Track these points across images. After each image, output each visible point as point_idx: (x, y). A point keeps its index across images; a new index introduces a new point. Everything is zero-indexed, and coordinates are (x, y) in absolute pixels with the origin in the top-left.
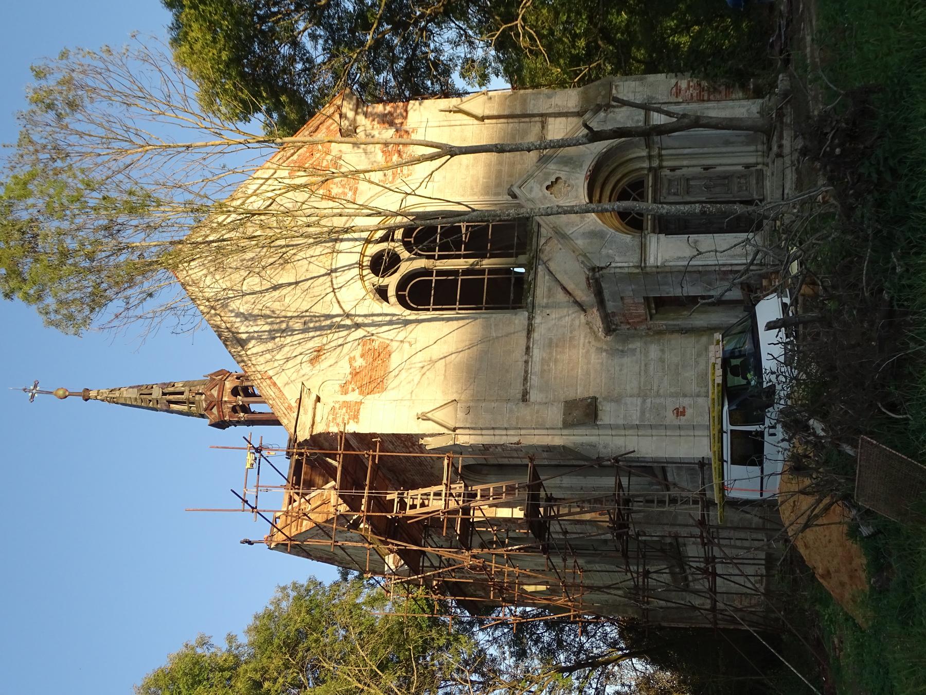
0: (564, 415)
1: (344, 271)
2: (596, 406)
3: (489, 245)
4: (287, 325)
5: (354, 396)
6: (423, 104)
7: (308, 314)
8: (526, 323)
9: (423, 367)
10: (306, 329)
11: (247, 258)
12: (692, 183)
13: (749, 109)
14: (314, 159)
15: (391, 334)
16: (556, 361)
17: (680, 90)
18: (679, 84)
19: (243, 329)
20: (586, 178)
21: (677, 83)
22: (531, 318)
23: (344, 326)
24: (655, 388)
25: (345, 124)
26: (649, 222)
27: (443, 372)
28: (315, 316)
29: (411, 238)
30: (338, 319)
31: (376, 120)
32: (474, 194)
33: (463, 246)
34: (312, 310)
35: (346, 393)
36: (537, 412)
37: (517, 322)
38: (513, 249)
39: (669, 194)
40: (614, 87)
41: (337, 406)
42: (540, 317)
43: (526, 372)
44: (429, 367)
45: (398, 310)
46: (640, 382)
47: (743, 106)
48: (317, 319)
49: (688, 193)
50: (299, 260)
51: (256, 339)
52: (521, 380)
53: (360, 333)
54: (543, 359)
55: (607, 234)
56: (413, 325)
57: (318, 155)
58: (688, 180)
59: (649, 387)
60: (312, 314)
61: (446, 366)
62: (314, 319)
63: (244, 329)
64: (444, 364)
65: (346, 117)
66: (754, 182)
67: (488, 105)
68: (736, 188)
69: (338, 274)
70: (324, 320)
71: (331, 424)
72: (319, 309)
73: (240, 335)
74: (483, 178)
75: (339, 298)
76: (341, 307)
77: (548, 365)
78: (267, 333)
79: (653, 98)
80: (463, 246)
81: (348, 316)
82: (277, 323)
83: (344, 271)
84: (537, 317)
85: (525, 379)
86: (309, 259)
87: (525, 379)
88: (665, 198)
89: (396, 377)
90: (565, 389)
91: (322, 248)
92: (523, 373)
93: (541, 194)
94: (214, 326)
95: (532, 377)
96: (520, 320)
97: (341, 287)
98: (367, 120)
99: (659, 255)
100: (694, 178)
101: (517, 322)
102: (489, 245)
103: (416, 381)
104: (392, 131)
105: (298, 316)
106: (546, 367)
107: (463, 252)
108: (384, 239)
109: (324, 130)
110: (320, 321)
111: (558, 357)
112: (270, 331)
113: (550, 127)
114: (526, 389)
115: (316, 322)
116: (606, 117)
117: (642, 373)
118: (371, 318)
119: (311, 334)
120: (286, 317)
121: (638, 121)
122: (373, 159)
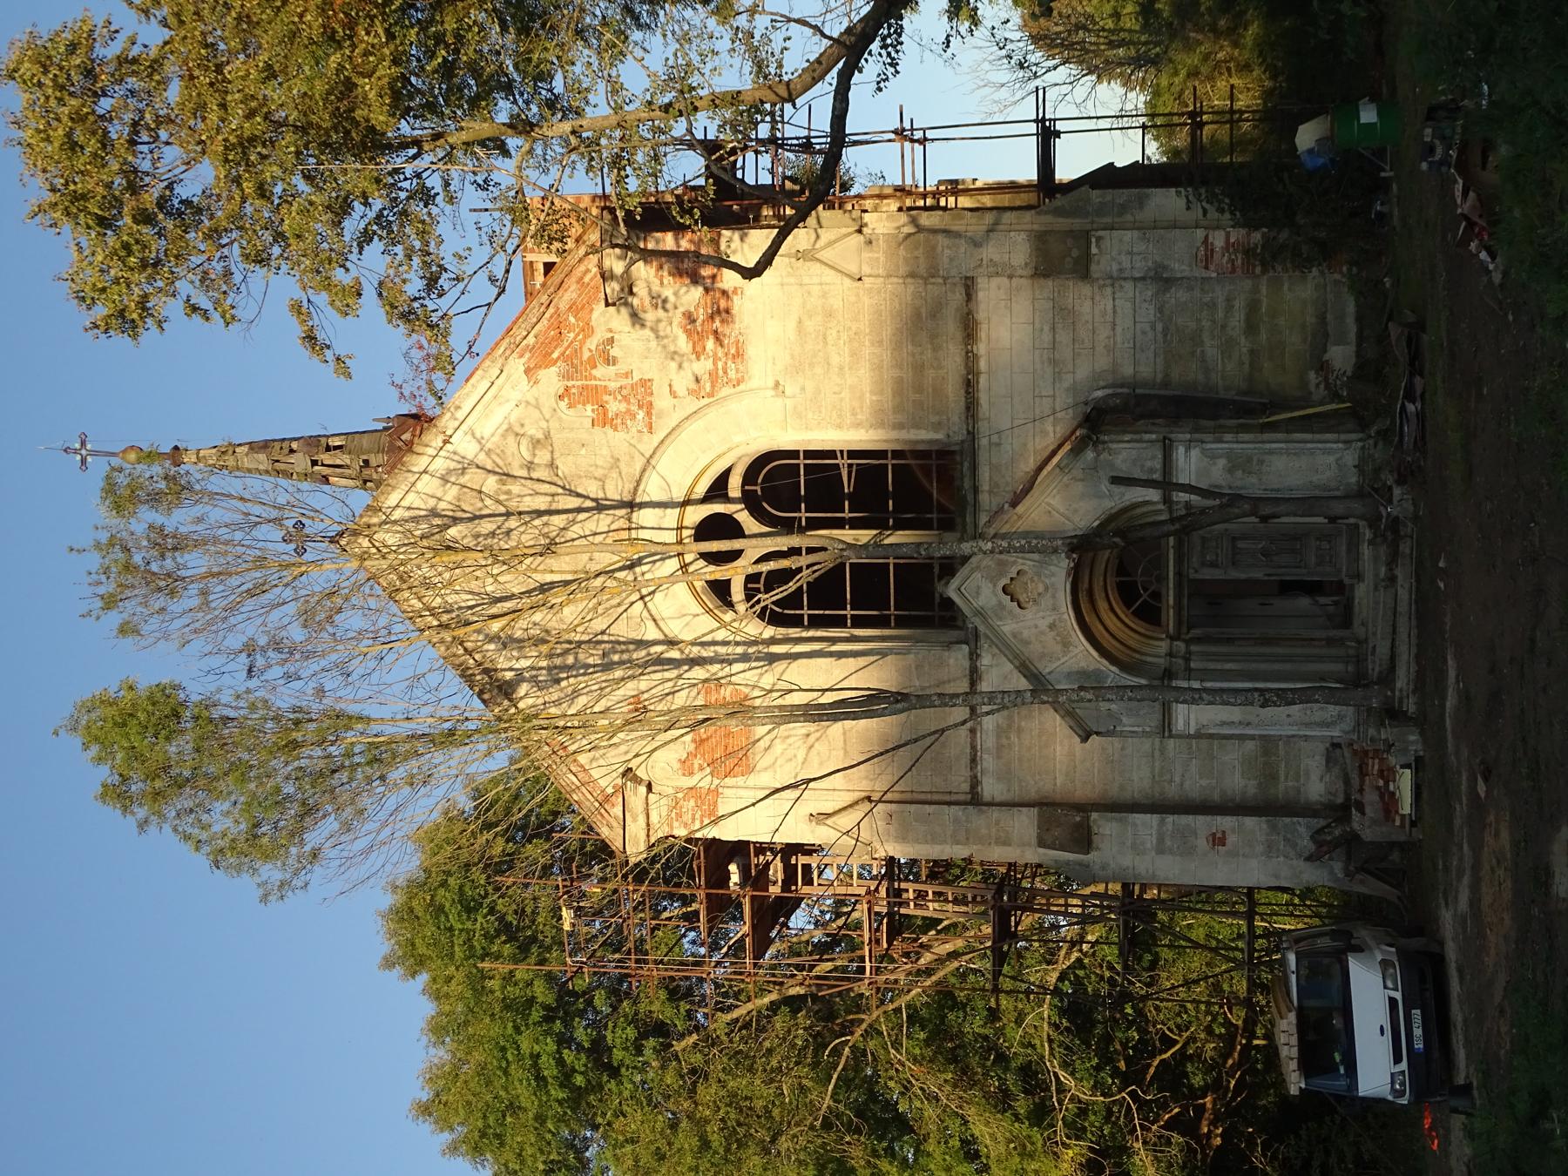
0: (1039, 828)
1: (654, 562)
2: (1089, 827)
3: (891, 502)
4: (576, 658)
5: (704, 780)
6: (747, 240)
7: (606, 638)
8: (967, 664)
9: (808, 735)
10: (607, 664)
11: (484, 532)
12: (1240, 544)
13: (1341, 458)
14: (566, 344)
15: (751, 676)
16: (1020, 730)
17: (1212, 250)
18: (1210, 240)
19: (502, 663)
20: (1068, 574)
21: (1206, 237)
22: (974, 656)
23: (670, 661)
24: (1177, 779)
25: (613, 290)
26: (1171, 611)
27: (841, 744)
28: (619, 643)
29: (756, 484)
30: (659, 649)
31: (666, 267)
32: (858, 425)
33: (847, 503)
34: (612, 630)
35: (691, 774)
36: (997, 823)
37: (952, 661)
38: (932, 513)
39: (1203, 564)
40: (1093, 240)
41: (680, 795)
42: (990, 656)
43: (973, 748)
44: (818, 734)
45: (756, 629)
46: (1153, 767)
47: (1329, 452)
48: (623, 647)
49: (1233, 564)
50: (573, 540)
51: (529, 681)
52: (966, 760)
53: (699, 673)
54: (998, 726)
55: (1107, 676)
56: (783, 664)
57: (572, 335)
58: (1234, 539)
59: (1168, 777)
60: (612, 638)
61: (844, 733)
62: (619, 648)
63: (507, 664)
64: (841, 730)
65: (613, 277)
66: (1344, 548)
67: (866, 255)
68: (1313, 559)
69: (645, 568)
70: (635, 650)
71: (676, 824)
72: (622, 630)
73: (500, 675)
74: (872, 392)
75: (654, 612)
76: (660, 629)
77: (1008, 738)
78: (544, 672)
79: (1165, 268)
80: (847, 503)
81: (671, 643)
82: (559, 655)
83: (654, 562)
84: (983, 654)
85: (973, 760)
86: (590, 538)
87: (973, 760)
88: (1196, 571)
89: (766, 749)
90: (1037, 777)
91: (610, 519)
92: (968, 751)
93: (994, 601)
94: (456, 667)
95: (985, 756)
96: (957, 659)
97: (653, 592)
98: (648, 267)
99: (1192, 716)
100: (1244, 537)
101: (952, 661)
102: (891, 502)
103: (800, 758)
104: (697, 292)
105: (589, 641)
106: (1004, 741)
107: (847, 515)
108: (708, 498)
109: (574, 287)
110: (628, 651)
111: (1023, 724)
112: (549, 669)
113: (981, 295)
114: (976, 777)
115: (622, 652)
116: (1096, 459)
117: (1157, 753)
118: (712, 648)
119: (618, 674)
120: (570, 642)
121: (1152, 470)
122: (672, 348)
